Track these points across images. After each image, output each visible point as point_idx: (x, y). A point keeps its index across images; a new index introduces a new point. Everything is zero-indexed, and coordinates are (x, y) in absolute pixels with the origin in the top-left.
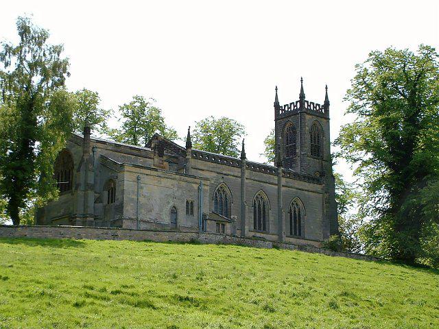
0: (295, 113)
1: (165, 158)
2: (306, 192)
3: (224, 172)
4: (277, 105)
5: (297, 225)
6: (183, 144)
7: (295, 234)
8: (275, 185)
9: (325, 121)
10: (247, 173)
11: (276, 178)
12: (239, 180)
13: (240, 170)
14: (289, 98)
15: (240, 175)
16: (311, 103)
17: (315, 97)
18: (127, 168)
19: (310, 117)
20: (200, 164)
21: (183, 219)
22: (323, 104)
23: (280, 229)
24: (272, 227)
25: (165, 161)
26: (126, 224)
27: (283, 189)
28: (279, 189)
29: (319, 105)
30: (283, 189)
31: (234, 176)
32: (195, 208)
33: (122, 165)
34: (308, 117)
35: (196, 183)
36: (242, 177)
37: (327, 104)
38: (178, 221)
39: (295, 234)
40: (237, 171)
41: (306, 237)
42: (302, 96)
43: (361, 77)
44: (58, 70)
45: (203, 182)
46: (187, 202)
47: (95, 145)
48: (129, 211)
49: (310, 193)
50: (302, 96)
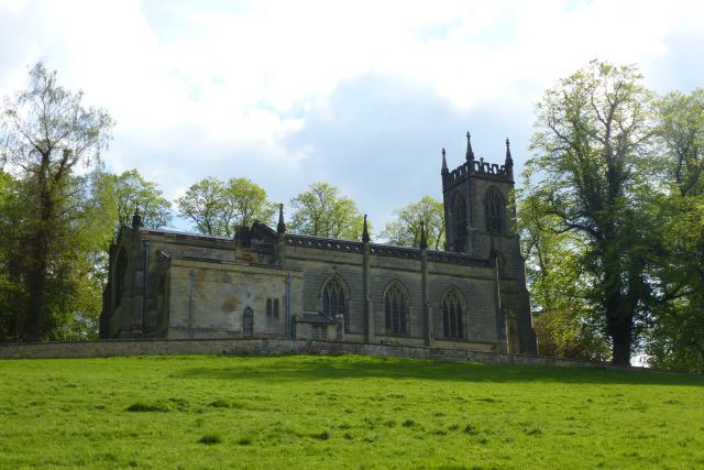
0: (489, 177)
1: (252, 249)
2: (469, 280)
3: (336, 260)
4: (445, 172)
5: (457, 324)
6: (275, 229)
7: (453, 335)
8: (419, 272)
9: (506, 185)
10: (373, 259)
11: (419, 263)
12: (360, 269)
13: (361, 256)
14: (456, 161)
15: (419, 268)
16: (493, 165)
17: (492, 156)
18: (173, 262)
19: (484, 182)
20: (300, 252)
21: (260, 324)
22: (504, 164)
23: (426, 331)
24: (414, 330)
25: (253, 251)
26: (172, 334)
27: (430, 278)
28: (365, 269)
29: (497, 166)
30: (430, 278)
31: (352, 264)
32: (282, 309)
33: (170, 259)
34: (480, 183)
35: (282, 276)
36: (364, 265)
37: (509, 162)
38: (255, 326)
39: (453, 335)
40: (357, 258)
41: (470, 337)
42: (470, 155)
43: (89, 130)
44: (89, 130)
45: (292, 273)
46: (269, 301)
47: (148, 237)
48: (177, 317)
49: (474, 280)
50: (470, 155)
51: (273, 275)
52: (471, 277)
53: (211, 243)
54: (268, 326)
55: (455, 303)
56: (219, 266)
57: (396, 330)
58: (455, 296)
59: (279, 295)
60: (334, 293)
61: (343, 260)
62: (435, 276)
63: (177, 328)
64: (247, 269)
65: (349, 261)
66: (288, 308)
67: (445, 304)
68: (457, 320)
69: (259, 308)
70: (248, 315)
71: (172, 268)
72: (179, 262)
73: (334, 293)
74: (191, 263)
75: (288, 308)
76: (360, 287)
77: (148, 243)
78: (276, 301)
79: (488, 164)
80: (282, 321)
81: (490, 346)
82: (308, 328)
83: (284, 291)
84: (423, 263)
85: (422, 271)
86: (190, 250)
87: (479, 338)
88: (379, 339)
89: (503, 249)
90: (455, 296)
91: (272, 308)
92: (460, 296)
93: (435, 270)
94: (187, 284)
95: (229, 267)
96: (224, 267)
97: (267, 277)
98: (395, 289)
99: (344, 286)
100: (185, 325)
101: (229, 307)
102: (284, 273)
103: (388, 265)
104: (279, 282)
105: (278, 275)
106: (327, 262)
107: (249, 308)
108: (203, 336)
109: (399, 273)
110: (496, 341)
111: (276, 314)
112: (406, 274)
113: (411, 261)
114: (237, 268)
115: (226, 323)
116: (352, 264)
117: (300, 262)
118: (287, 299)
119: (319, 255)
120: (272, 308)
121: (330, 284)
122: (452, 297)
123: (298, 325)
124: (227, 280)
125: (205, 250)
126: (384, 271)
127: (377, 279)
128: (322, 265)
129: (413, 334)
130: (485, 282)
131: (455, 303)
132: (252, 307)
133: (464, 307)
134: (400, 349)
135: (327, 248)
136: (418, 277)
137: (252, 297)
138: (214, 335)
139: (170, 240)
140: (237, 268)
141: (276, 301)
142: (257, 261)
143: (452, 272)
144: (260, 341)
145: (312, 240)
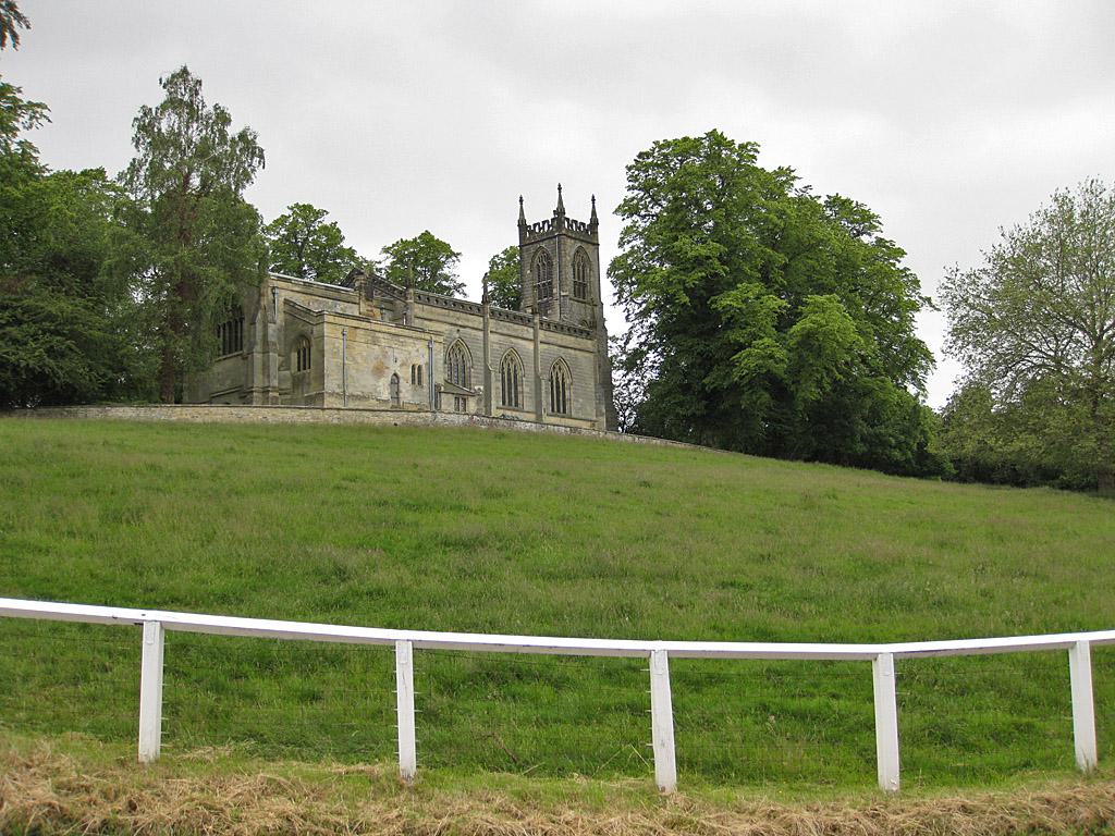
1: (375, 303)
2: (572, 352)
11: (531, 330)
15: (481, 327)
16: (544, 222)
18: (327, 318)
21: (407, 393)
23: (538, 404)
24: (528, 403)
26: (329, 402)
27: (541, 347)
28: (485, 335)
30: (492, 337)
31: (473, 328)
32: (425, 377)
36: (484, 330)
37: (595, 223)
38: (401, 395)
42: (560, 212)
48: (332, 383)
49: (577, 352)
50: (560, 212)
51: (417, 339)
53: (336, 295)
54: (413, 396)
55: (512, 367)
57: (510, 404)
58: (560, 369)
59: (422, 361)
61: (466, 324)
62: (546, 346)
63: (332, 394)
64: (393, 330)
65: (470, 325)
66: (430, 375)
68: (227, 339)
69: (405, 374)
71: (325, 325)
72: (331, 319)
75: (430, 375)
76: (481, 354)
77: (277, 291)
79: (568, 219)
80: (426, 390)
83: (426, 357)
84: (535, 331)
85: (534, 340)
87: (580, 416)
88: (501, 412)
90: (560, 369)
91: (417, 375)
94: (339, 343)
95: (377, 328)
97: (411, 341)
100: (337, 391)
101: (379, 371)
103: (505, 332)
104: (422, 346)
106: (452, 324)
107: (395, 375)
109: (513, 340)
110: (594, 418)
114: (384, 329)
116: (473, 328)
117: (426, 322)
118: (429, 365)
119: (439, 314)
122: (557, 370)
123: (443, 395)
124: (375, 342)
126: (502, 338)
127: (496, 347)
129: (526, 409)
130: (587, 355)
131: (512, 367)
132: (399, 373)
133: (568, 381)
136: (530, 346)
137: (399, 363)
139: (297, 289)
140: (384, 329)
143: (559, 342)
144: (429, 414)
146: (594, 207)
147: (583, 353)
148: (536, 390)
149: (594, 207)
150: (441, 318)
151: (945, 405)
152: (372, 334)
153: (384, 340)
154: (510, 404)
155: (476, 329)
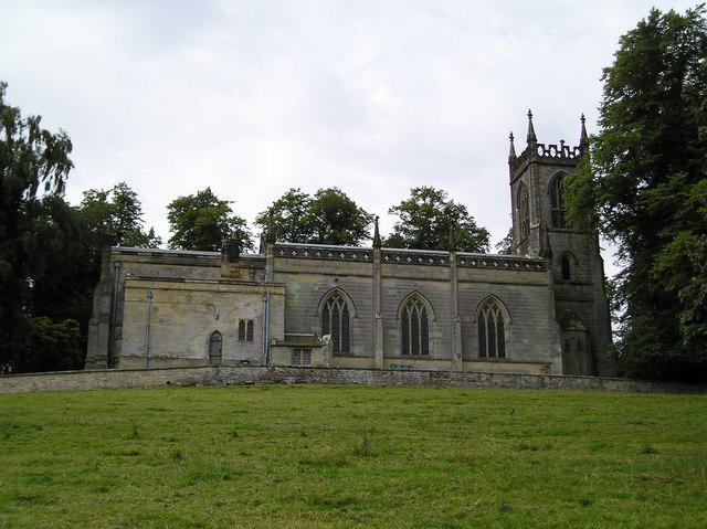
2: (514, 288)
16: (551, 146)
21: (232, 350)
31: (358, 276)
42: (532, 138)
45: (273, 290)
46: (242, 323)
48: (131, 344)
49: (519, 287)
50: (532, 138)
52: (517, 284)
53: (190, 261)
55: (495, 316)
56: (182, 286)
57: (492, 354)
60: (336, 310)
61: (349, 272)
67: (481, 317)
70: (215, 339)
72: (134, 283)
73: (336, 310)
74: (149, 284)
78: (251, 323)
79: (543, 146)
81: (540, 367)
82: (288, 352)
86: (168, 269)
87: (525, 358)
89: (575, 248)
92: (501, 306)
93: (467, 278)
96: (188, 287)
98: (336, 299)
99: (427, 304)
100: (139, 353)
102: (261, 289)
103: (407, 274)
105: (252, 293)
106: (326, 274)
108: (160, 365)
109: (420, 283)
111: (250, 338)
112: (429, 283)
113: (437, 268)
115: (188, 351)
116: (358, 276)
120: (246, 331)
121: (331, 301)
125: (185, 268)
126: (402, 282)
128: (315, 279)
131: (495, 316)
134: (389, 373)
135: (472, 267)
138: (174, 364)
139: (146, 260)
141: (251, 323)
142: (247, 278)
143: (491, 279)
145: (508, 261)
146: (584, 126)
147: (531, 288)
148: (403, 339)
149: (584, 126)
150: (312, 270)
151: (615, 59)
152: (187, 293)
153: (157, 296)
154: (492, 354)
155: (363, 276)
